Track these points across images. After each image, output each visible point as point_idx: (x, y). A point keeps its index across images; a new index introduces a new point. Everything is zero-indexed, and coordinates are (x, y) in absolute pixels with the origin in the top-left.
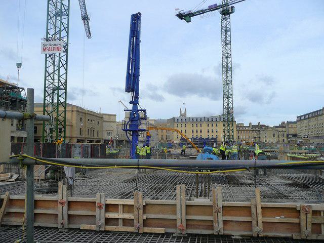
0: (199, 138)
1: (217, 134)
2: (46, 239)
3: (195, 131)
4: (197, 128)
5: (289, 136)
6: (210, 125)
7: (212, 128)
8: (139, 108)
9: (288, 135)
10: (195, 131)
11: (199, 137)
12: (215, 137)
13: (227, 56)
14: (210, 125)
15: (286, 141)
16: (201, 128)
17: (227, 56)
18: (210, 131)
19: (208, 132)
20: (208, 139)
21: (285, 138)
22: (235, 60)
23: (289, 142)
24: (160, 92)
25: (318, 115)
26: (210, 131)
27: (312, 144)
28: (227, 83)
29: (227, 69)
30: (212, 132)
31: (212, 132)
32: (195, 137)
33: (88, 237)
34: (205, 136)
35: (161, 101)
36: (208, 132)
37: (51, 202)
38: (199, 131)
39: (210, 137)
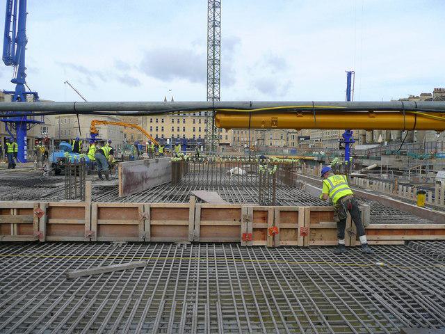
0: (181, 139)
1: (157, 133)
2: (13, 273)
3: (176, 129)
4: (157, 125)
5: (301, 139)
6: (197, 121)
7: (157, 125)
8: (27, 90)
9: (299, 138)
10: (176, 129)
11: (181, 137)
12: (202, 137)
13: (214, 25)
14: (197, 121)
15: (296, 145)
16: (184, 125)
17: (214, 25)
18: (197, 129)
19: (173, 130)
20: (193, 140)
21: (296, 141)
22: (226, 32)
23: (300, 146)
24: (133, 74)
25: (401, 110)
26: (197, 129)
27: (323, 149)
28: (214, 62)
29: (214, 43)
30: (178, 130)
31: (178, 130)
32: (176, 137)
33: (52, 273)
34: (189, 136)
35: (136, 85)
36: (173, 130)
37: (213, 227)
38: (181, 129)
39: (197, 137)
